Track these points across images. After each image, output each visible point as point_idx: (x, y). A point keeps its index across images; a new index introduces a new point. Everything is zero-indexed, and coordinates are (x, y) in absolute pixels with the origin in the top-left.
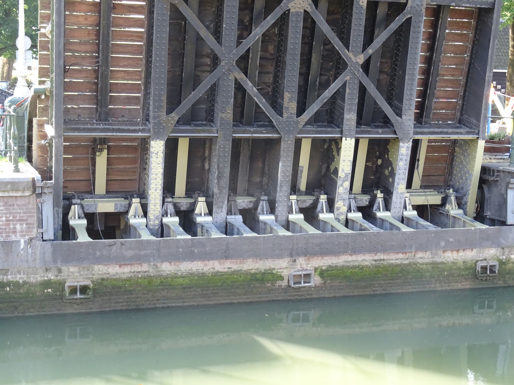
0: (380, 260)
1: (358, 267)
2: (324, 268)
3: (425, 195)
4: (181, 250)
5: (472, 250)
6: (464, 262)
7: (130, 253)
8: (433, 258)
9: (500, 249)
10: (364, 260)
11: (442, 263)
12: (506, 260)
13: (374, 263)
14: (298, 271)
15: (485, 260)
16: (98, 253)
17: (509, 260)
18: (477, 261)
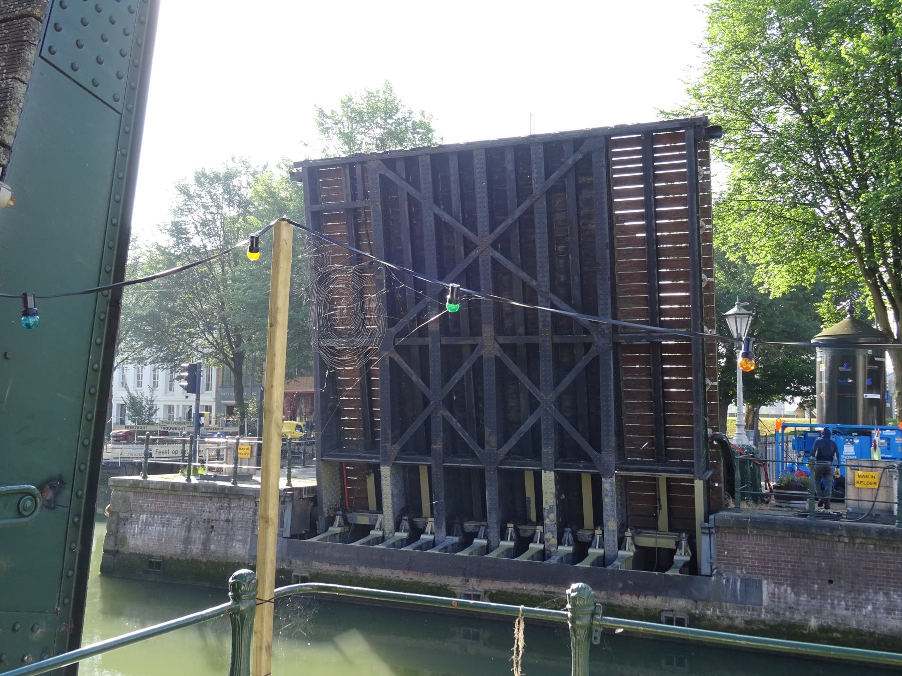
0: (551, 592)
1: (527, 595)
2: (494, 592)
3: (656, 538)
4: (374, 557)
5: (656, 597)
6: (645, 609)
7: (337, 555)
8: (608, 599)
9: (691, 601)
10: (533, 589)
11: (619, 606)
12: (700, 615)
13: (544, 594)
14: (469, 590)
15: (672, 611)
16: (316, 552)
17: (703, 616)
18: (662, 611)
